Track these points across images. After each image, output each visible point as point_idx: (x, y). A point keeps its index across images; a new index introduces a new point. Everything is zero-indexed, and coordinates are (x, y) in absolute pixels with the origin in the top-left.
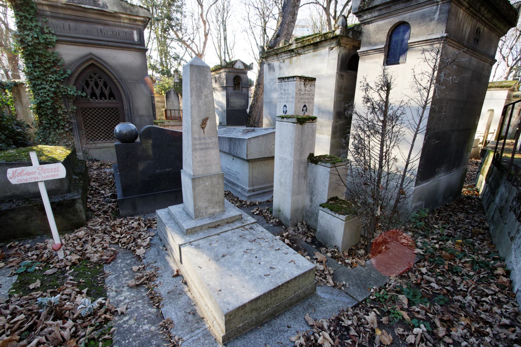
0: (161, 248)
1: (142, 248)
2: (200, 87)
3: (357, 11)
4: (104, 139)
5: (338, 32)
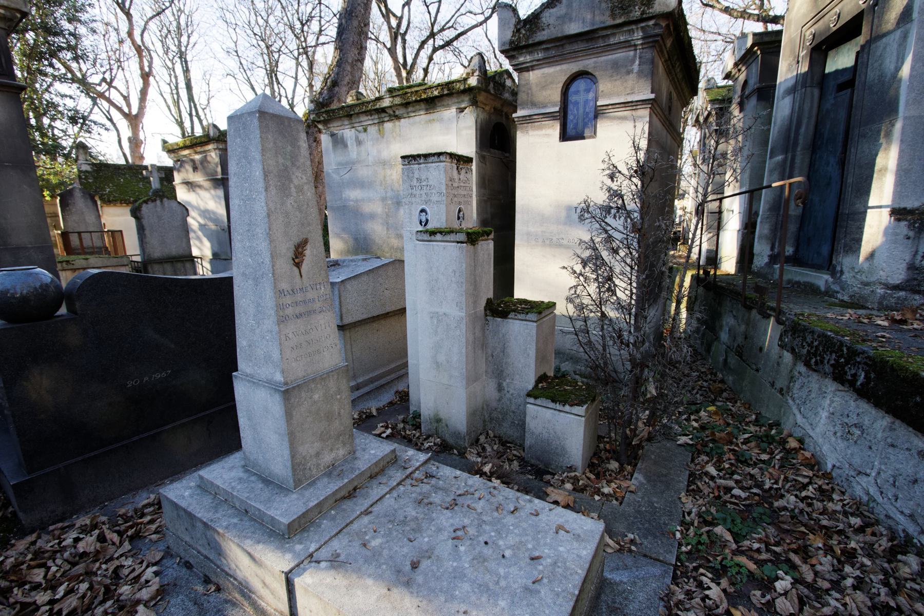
0: (200, 588)
1: (141, 608)
2: (286, 169)
3: (507, 47)
5: (473, 81)
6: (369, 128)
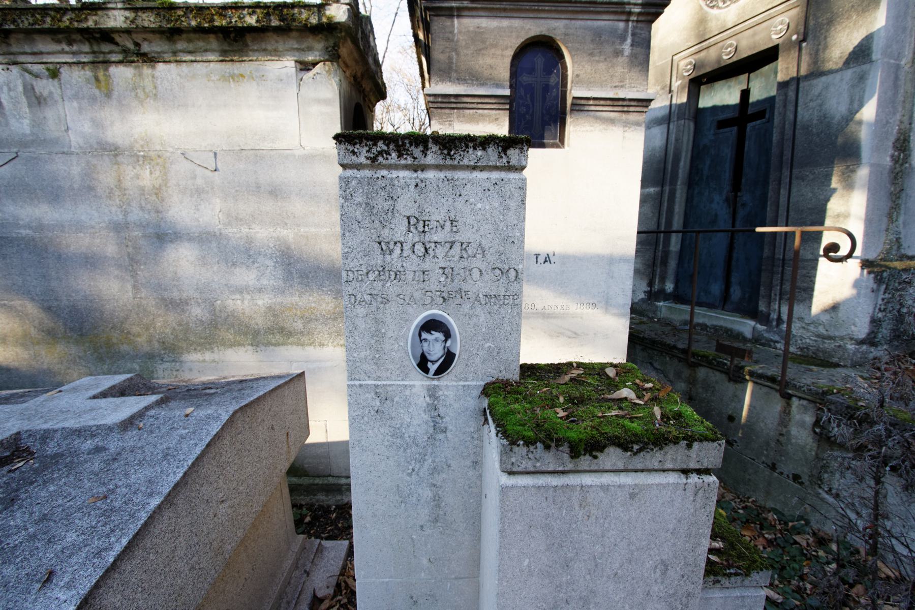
6: (65, 71)
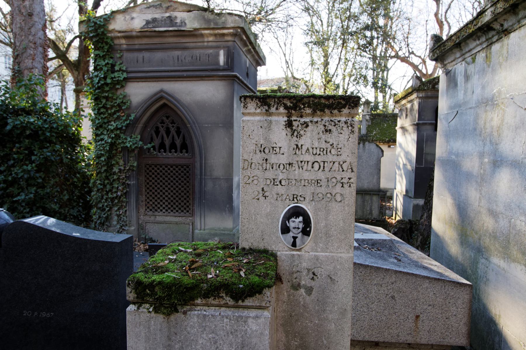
4: (167, 210)
